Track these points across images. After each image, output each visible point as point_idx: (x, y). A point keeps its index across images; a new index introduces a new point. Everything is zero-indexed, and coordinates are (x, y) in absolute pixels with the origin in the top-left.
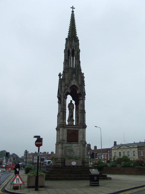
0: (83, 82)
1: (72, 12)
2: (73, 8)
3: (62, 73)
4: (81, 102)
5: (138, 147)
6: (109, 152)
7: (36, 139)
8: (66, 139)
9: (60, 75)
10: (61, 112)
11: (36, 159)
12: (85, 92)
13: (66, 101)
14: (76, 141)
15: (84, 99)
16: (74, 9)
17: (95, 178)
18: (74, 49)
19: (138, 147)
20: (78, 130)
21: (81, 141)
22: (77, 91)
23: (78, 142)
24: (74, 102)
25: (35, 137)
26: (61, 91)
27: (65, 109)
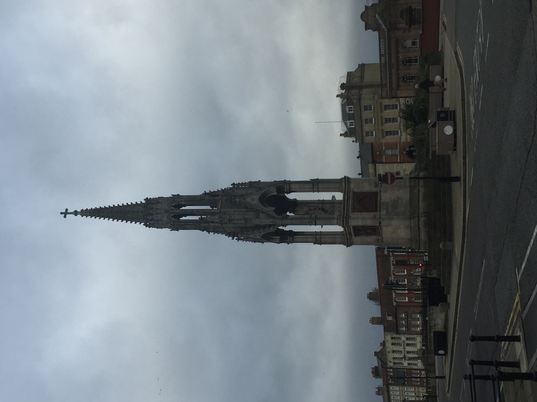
0: (252, 185)
1: (76, 215)
2: (65, 213)
5: (374, 162)
8: (372, 214)
13: (300, 200)
14: (374, 196)
18: (175, 205)
19: (374, 162)
21: (376, 185)
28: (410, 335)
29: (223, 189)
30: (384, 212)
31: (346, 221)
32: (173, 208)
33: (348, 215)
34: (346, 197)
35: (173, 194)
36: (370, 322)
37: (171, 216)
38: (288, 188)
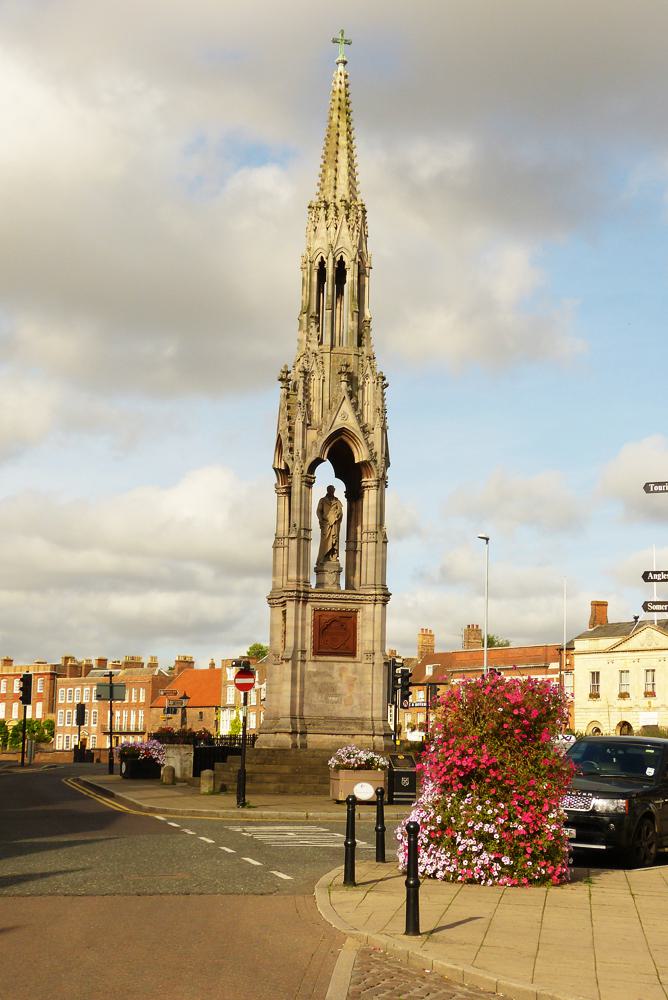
4: (370, 498)
17: (405, 781)
20: (356, 611)
22: (356, 455)
32: (338, 259)
38: (369, 484)
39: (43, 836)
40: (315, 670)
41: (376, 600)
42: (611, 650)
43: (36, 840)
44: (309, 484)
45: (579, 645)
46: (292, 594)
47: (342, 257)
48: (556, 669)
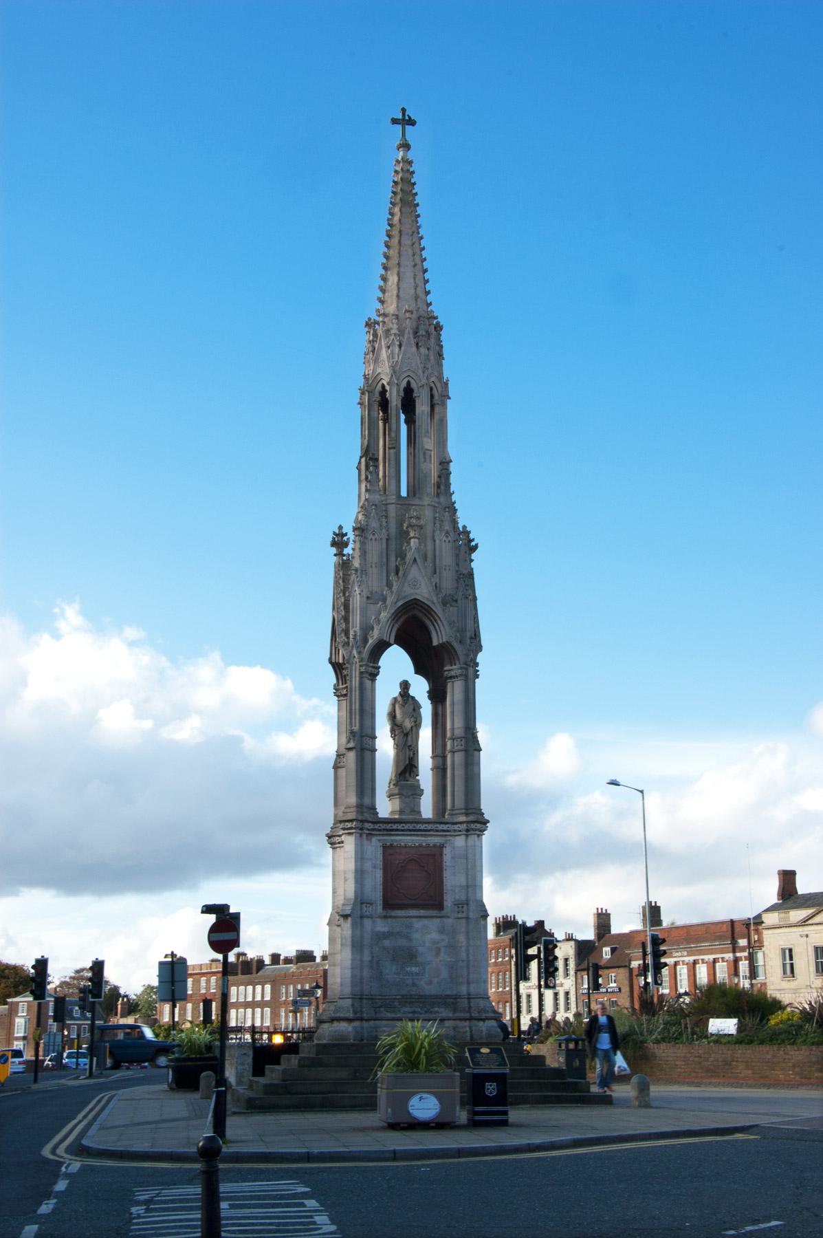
3: (348, 529)
4: (455, 692)
6: (743, 949)
7: (212, 919)
9: (339, 542)
10: (349, 749)
11: (237, 1005)
12: (476, 636)
14: (433, 900)
15: (470, 672)
16: (408, 128)
20: (442, 846)
23: (440, 906)
24: (420, 688)
25: (208, 909)
26: (347, 632)
27: (369, 732)
28: (575, 999)
29: (455, 505)
30: (381, 926)
31: (351, 828)
32: (404, 384)
33: (373, 833)
34: (424, 825)
35: (449, 382)
36: (598, 909)
37: (411, 379)
38: (453, 673)
39: (56, 1160)
40: (385, 929)
41: (467, 830)
42: (804, 922)
43: (528, 1081)
44: (372, 674)
45: (770, 919)
46: (349, 825)
47: (409, 383)
48: (744, 946)
